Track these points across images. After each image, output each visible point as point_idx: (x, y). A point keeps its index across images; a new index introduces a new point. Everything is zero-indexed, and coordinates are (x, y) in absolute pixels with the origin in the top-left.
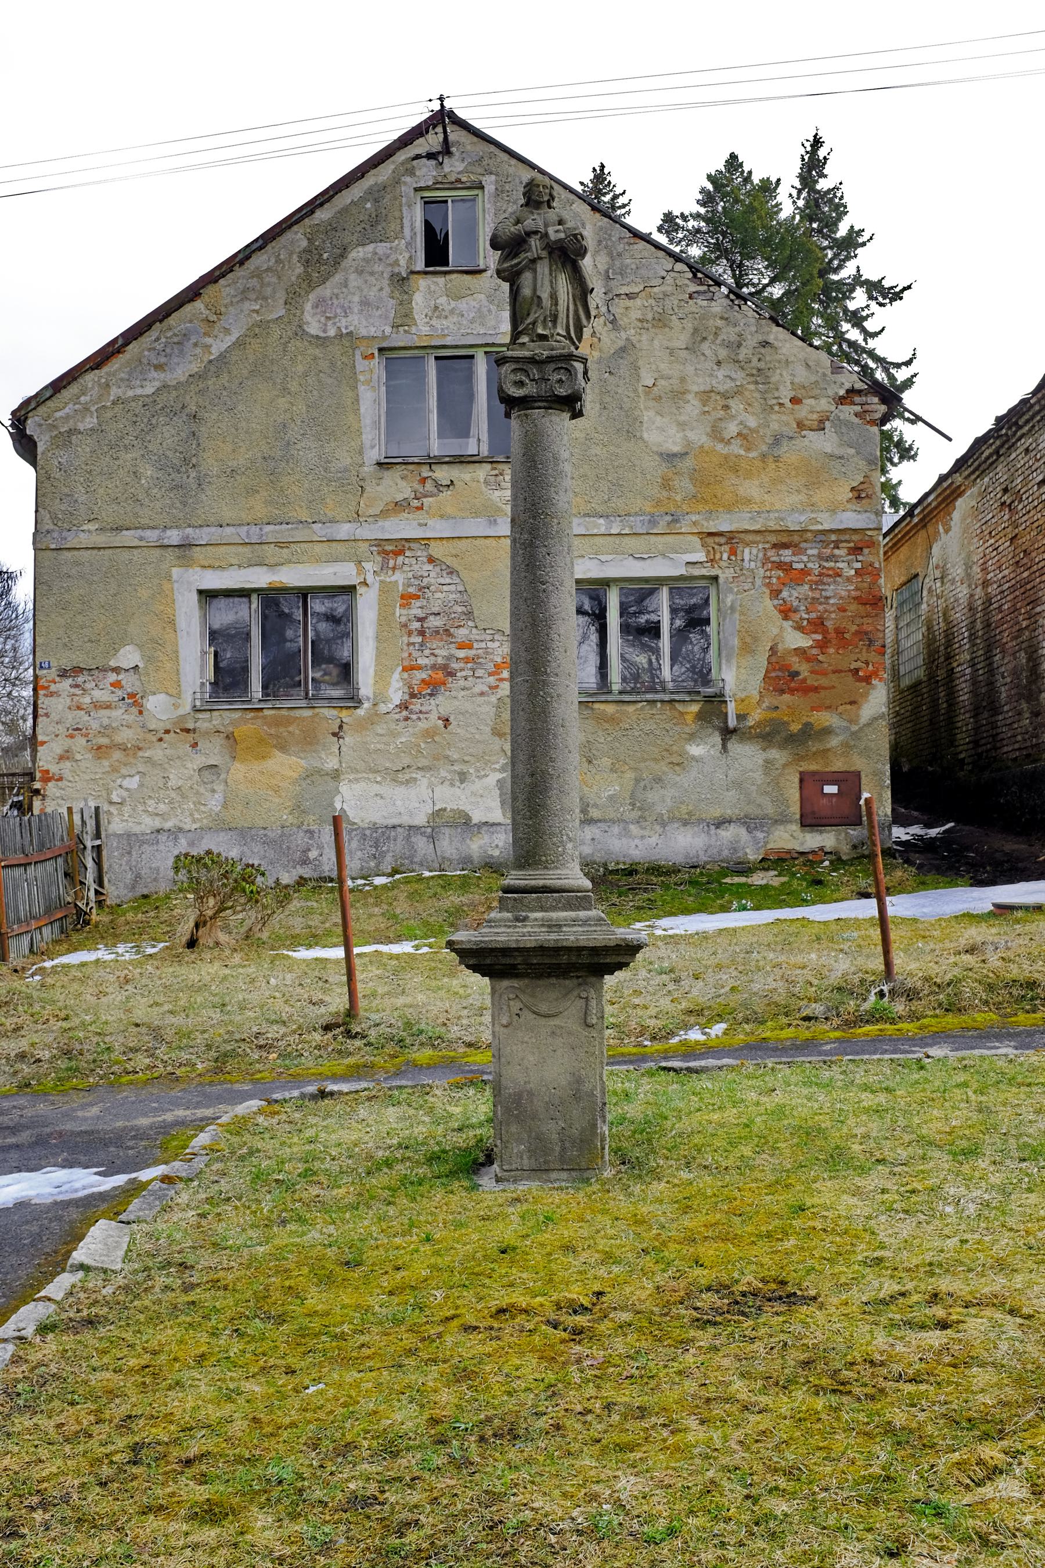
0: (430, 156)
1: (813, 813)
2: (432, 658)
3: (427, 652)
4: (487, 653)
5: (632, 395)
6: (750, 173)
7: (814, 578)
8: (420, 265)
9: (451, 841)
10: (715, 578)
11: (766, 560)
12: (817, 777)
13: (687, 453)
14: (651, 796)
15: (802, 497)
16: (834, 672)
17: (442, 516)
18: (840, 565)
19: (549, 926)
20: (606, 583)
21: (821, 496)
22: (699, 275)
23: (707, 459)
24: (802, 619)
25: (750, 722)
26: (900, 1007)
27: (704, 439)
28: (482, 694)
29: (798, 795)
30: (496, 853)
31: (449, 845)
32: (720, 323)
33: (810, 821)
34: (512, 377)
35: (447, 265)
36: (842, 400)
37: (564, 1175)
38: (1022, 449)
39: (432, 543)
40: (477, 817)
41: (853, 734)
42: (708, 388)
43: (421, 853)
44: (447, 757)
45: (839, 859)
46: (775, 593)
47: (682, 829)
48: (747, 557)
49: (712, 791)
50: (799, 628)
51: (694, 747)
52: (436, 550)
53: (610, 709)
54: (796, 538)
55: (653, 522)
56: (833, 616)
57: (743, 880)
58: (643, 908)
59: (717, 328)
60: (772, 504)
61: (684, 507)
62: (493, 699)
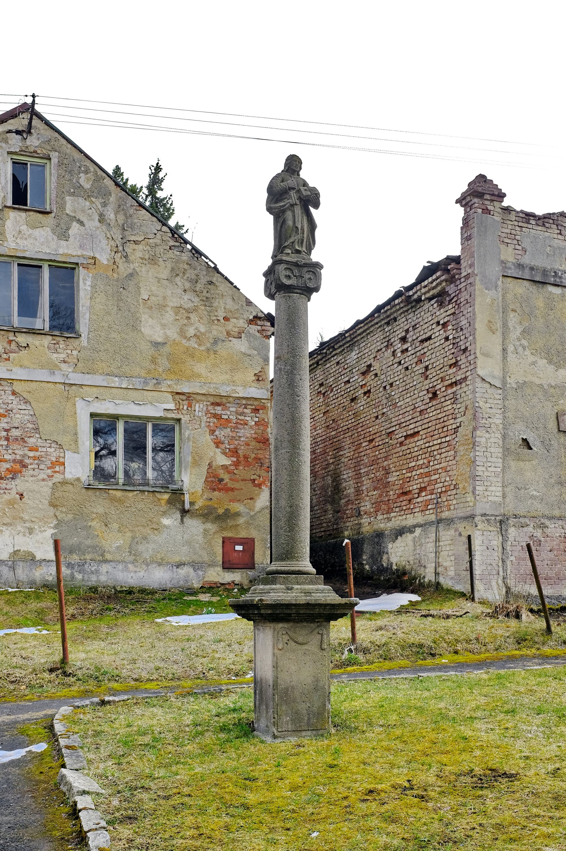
0: (18, 132)
1: (229, 561)
2: (13, 455)
3: (10, 451)
4: (47, 455)
5: (136, 304)
6: (127, 180)
7: (233, 425)
8: (9, 203)
9: (23, 570)
10: (179, 420)
11: (207, 412)
12: (231, 541)
13: (166, 343)
14: (141, 548)
15: (228, 376)
16: (242, 480)
17: (21, 366)
18: (247, 418)
19: (305, 593)
20: (117, 417)
21: (238, 377)
22: (176, 236)
23: (177, 348)
24: (226, 448)
25: (197, 507)
26: (361, 657)
27: (176, 336)
28: (43, 480)
29: (221, 550)
30: (50, 579)
31: (22, 573)
32: (186, 267)
33: (227, 566)
34: (284, 272)
35: (26, 205)
36: (251, 322)
37: (309, 733)
38: (334, 362)
39: (15, 383)
40: (39, 556)
41: (251, 516)
42: (179, 305)
43: (5, 577)
44: (21, 518)
45: (243, 588)
46: (212, 432)
47: (158, 568)
48: (197, 409)
49: (170, 547)
50: (224, 453)
51: (165, 519)
52: (17, 387)
53: (119, 494)
54: (224, 400)
55: (146, 383)
56: (242, 447)
57: (194, 598)
58: (151, 612)
59: (184, 269)
60: (212, 379)
61: (163, 375)
62: (50, 484)
